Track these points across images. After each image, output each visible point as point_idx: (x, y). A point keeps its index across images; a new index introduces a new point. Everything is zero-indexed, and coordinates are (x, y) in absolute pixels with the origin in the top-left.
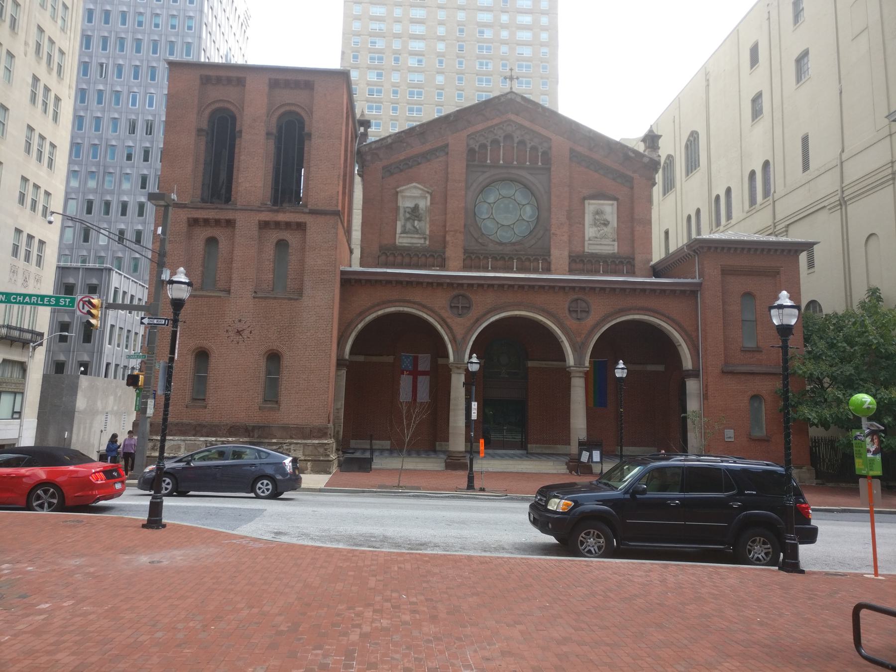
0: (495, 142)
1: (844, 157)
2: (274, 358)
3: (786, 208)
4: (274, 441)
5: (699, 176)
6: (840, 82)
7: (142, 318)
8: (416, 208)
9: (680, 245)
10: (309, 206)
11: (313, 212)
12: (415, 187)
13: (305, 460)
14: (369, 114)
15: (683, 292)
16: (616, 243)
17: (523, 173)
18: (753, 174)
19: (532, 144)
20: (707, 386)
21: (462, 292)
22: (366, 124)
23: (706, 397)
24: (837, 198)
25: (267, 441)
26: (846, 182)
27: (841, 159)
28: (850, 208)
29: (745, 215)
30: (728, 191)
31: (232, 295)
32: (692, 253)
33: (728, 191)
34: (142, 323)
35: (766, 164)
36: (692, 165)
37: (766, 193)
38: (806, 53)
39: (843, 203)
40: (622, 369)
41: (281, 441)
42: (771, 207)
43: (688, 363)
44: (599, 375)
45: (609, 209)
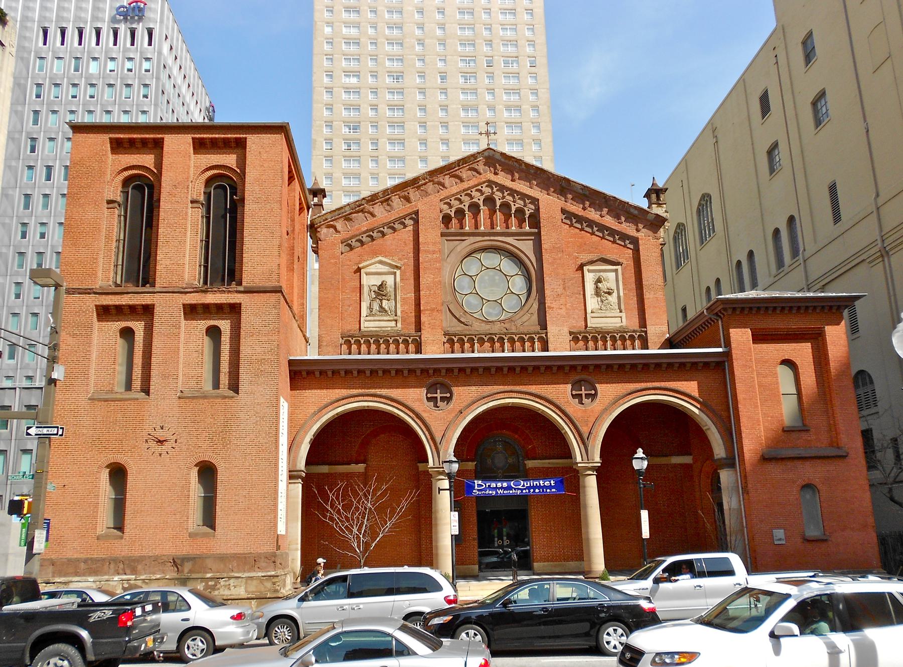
0: (474, 208)
1: (880, 201)
2: (207, 473)
3: (818, 267)
4: (209, 575)
5: (715, 245)
6: (865, 120)
7: (28, 428)
8: (382, 286)
9: (699, 309)
10: (244, 284)
11: (248, 291)
12: (381, 262)
13: (248, 599)
14: (324, 184)
15: (706, 365)
16: (623, 315)
17: (510, 240)
18: (777, 232)
19: (517, 206)
20: (746, 477)
21: (440, 379)
22: (319, 193)
23: (745, 490)
24: (876, 249)
25: (199, 576)
26: (885, 230)
27: (876, 204)
28: (893, 259)
29: (772, 280)
30: (751, 254)
31: (152, 396)
32: (713, 317)
33: (751, 254)
34: (28, 434)
35: (791, 219)
36: (705, 233)
37: (795, 252)
38: (822, 94)
39: (884, 254)
40: (642, 458)
41: (218, 575)
42: (802, 268)
43: (719, 450)
44: (613, 471)
45: (610, 278)
